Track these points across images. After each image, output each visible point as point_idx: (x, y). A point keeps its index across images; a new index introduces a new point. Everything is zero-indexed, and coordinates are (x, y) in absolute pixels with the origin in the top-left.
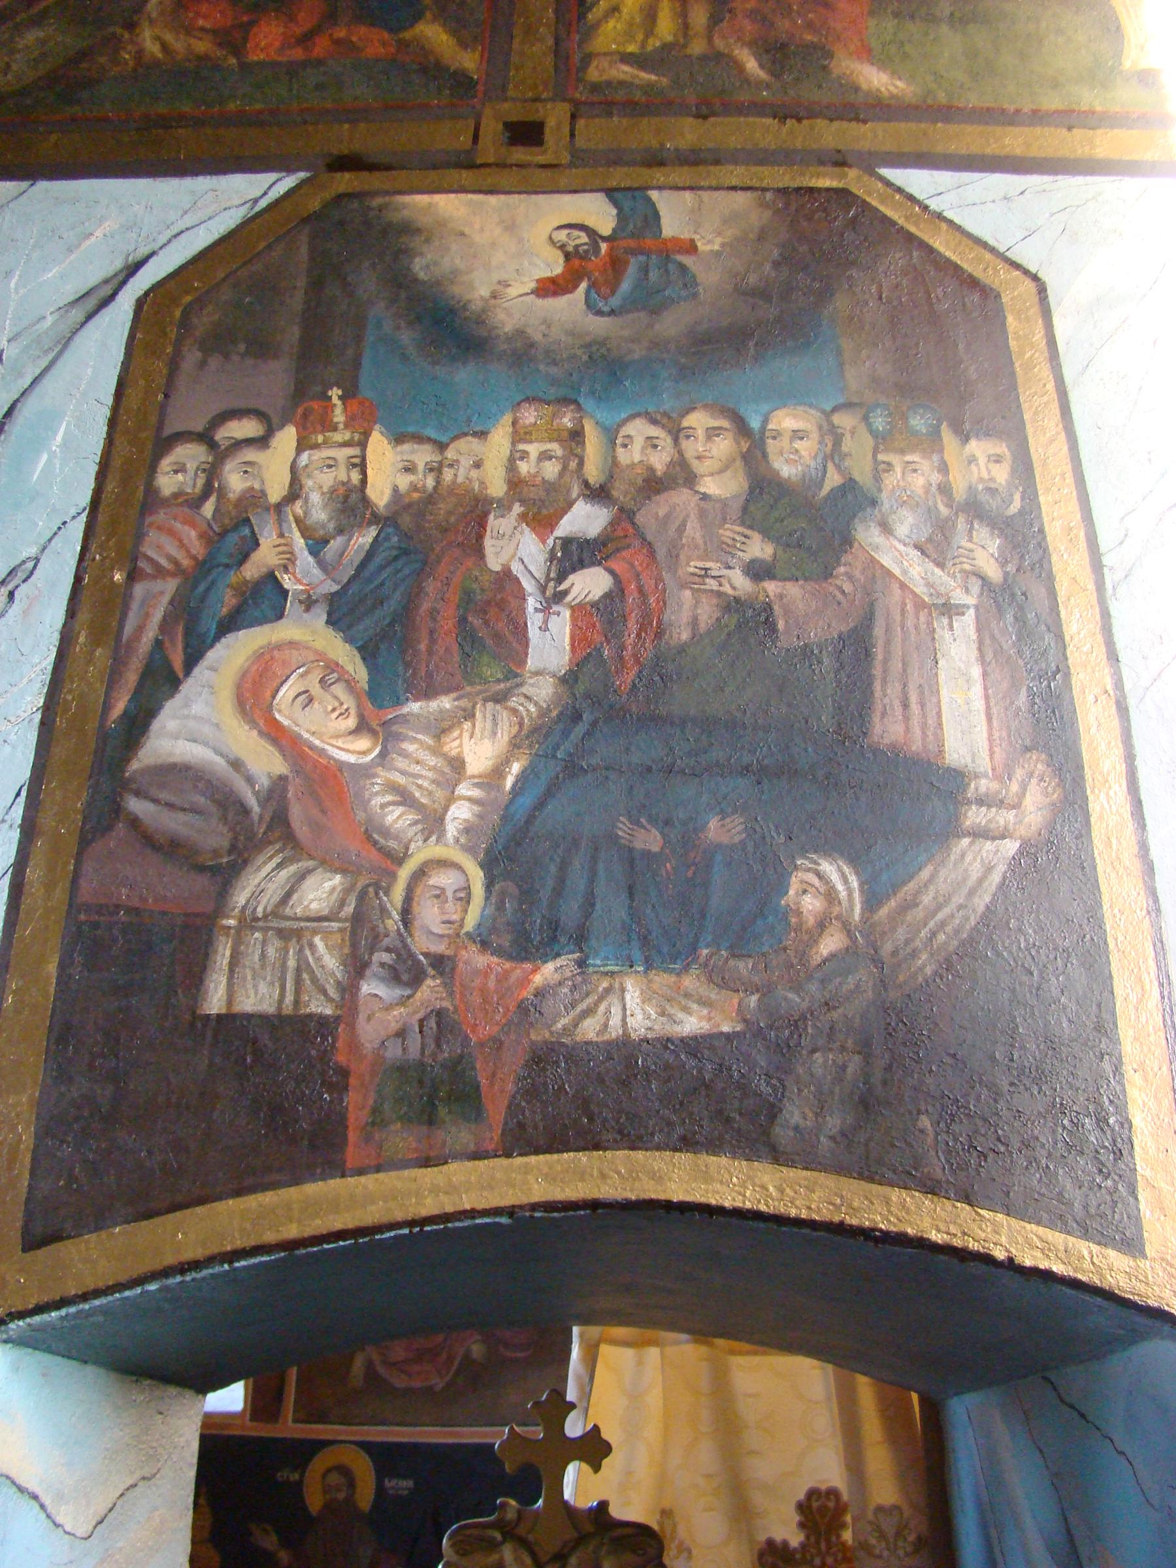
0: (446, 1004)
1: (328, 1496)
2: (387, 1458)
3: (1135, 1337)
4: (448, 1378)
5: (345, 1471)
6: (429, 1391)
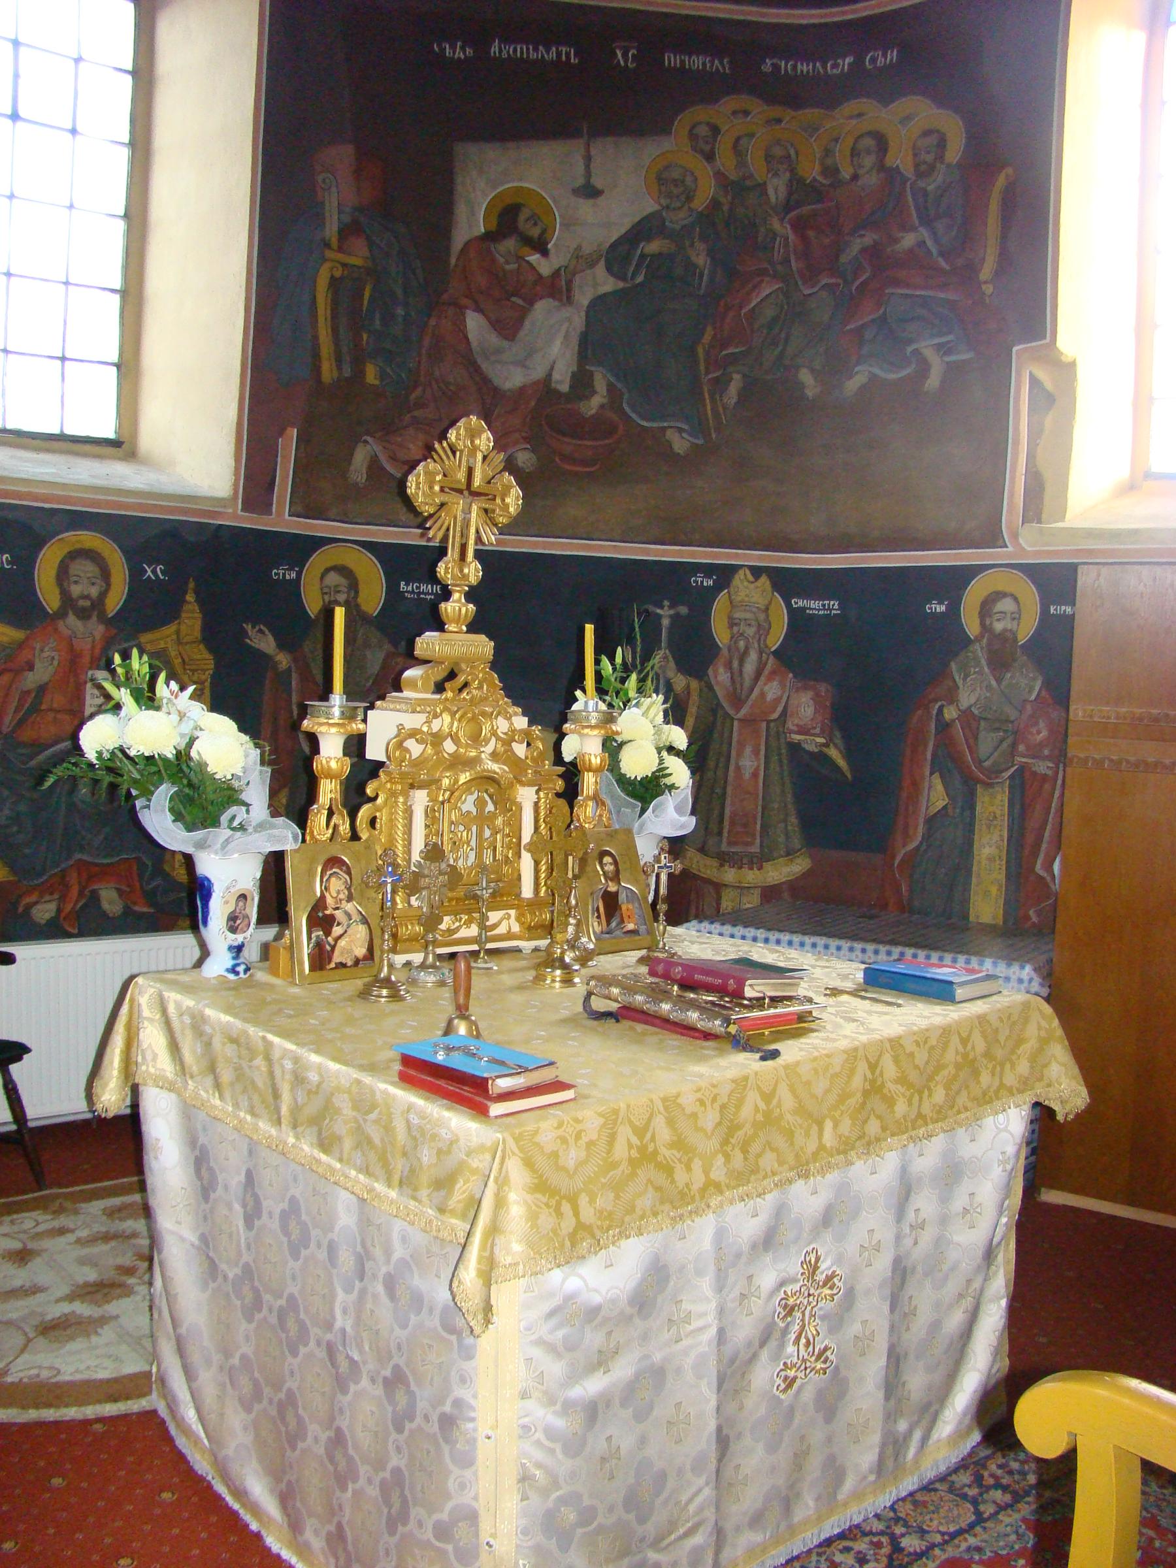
0: (859, 183)
1: (327, 598)
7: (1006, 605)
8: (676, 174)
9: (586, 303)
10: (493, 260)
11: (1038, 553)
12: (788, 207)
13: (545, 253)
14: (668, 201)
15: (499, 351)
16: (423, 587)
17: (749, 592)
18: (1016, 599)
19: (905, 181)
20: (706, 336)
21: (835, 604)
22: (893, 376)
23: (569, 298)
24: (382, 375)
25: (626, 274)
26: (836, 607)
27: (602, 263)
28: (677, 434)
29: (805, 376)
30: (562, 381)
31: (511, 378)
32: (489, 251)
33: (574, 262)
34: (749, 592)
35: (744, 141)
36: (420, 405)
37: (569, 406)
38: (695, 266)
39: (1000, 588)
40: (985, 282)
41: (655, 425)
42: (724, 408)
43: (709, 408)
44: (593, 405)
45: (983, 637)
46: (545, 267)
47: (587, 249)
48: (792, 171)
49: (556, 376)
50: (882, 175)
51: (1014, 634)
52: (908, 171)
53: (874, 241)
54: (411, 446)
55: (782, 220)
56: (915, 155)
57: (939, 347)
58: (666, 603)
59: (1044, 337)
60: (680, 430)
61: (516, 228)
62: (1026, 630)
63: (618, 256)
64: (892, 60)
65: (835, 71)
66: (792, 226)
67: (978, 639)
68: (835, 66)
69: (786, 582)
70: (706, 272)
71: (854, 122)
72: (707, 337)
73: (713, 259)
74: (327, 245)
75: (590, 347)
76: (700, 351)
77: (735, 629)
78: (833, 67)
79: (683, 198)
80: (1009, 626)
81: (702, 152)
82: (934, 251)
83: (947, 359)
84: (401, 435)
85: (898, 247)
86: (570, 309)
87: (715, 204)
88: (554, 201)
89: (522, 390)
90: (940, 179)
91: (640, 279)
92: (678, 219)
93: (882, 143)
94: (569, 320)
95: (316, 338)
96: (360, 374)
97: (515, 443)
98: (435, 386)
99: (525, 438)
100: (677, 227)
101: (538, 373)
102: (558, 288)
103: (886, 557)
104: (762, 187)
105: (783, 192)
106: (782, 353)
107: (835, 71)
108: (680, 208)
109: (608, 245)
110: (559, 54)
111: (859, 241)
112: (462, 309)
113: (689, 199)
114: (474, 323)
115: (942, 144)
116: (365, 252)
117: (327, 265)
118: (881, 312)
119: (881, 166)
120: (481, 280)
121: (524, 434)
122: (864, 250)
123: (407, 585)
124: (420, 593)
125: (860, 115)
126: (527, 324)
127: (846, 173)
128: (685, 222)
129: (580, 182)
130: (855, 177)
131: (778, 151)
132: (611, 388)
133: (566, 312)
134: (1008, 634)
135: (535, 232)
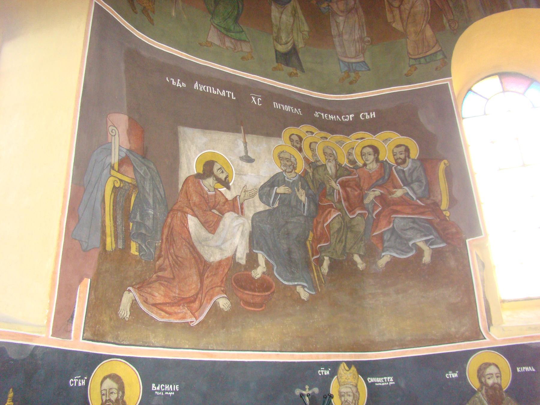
0: (368, 167)
2: (150, 370)
3: (279, 52)
4: (202, 318)
5: (116, 378)
6: (186, 326)
7: (492, 370)
8: (287, 156)
9: (251, 215)
10: (202, 189)
11: (504, 340)
12: (337, 177)
13: (229, 188)
14: (285, 168)
15: (206, 240)
16: (167, 387)
17: (347, 375)
18: (497, 366)
19: (391, 166)
20: (310, 237)
21: (390, 379)
22: (405, 257)
23: (242, 212)
24: (140, 249)
25: (269, 203)
26: (392, 380)
27: (257, 196)
28: (302, 289)
29: (357, 258)
30: (242, 257)
31: (214, 256)
32: (199, 183)
33: (243, 193)
34: (347, 375)
35: (313, 145)
36: (161, 269)
37: (246, 273)
38: (301, 201)
39: (487, 361)
40: (445, 210)
41: (290, 284)
42: (323, 275)
43: (315, 274)
44: (258, 273)
45: (482, 388)
46: (229, 195)
47: (249, 188)
48: (336, 160)
49: (238, 255)
50: (379, 164)
51: (500, 386)
52: (392, 161)
53: (381, 193)
54: (156, 294)
55: (336, 182)
56: (394, 155)
57: (426, 241)
58: (307, 387)
59: (481, 234)
60: (304, 287)
61: (213, 173)
62: (506, 381)
63: (266, 190)
64: (373, 116)
65: (346, 120)
66: (340, 185)
67: (480, 390)
68: (345, 118)
69: (365, 369)
70: (306, 204)
71: (360, 141)
72: (310, 238)
73: (308, 198)
74: (113, 167)
75: (255, 239)
76: (308, 243)
77: (343, 399)
78: (345, 118)
79: (291, 167)
80: (496, 381)
81: (296, 147)
82: (414, 198)
83: (432, 247)
84: (150, 287)
85: (394, 196)
86: (243, 219)
87: (306, 172)
88: (231, 161)
89: (220, 262)
90: (410, 166)
91: (276, 205)
92: (291, 177)
93: (376, 151)
94: (243, 224)
95: (103, 222)
96: (127, 247)
97: (218, 293)
98: (171, 258)
99: (223, 291)
100: (291, 181)
101: (228, 254)
102: (236, 206)
103: (416, 350)
104: (324, 166)
105: (334, 171)
106: (345, 246)
107: (346, 120)
108: (291, 172)
109: (259, 187)
110: (226, 94)
111: (373, 193)
112: (186, 213)
113: (295, 168)
114: (193, 223)
115: (407, 150)
116: (132, 175)
117: (112, 179)
118: (391, 226)
119: (377, 160)
120: (195, 198)
121: (222, 289)
122: (375, 197)
123: (157, 386)
124: (164, 392)
125: (362, 138)
126: (221, 226)
127: (360, 163)
128: (294, 179)
129: (243, 154)
130: (365, 165)
131: (329, 151)
132: (267, 262)
133: (241, 220)
134: (496, 386)
135: (222, 176)
